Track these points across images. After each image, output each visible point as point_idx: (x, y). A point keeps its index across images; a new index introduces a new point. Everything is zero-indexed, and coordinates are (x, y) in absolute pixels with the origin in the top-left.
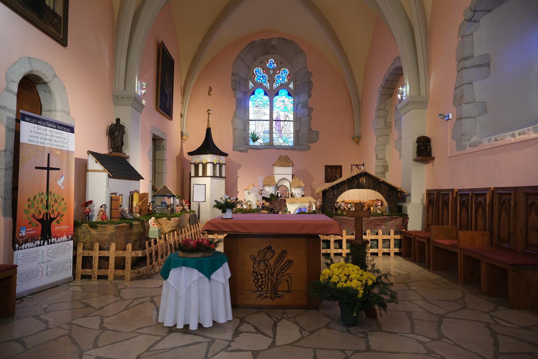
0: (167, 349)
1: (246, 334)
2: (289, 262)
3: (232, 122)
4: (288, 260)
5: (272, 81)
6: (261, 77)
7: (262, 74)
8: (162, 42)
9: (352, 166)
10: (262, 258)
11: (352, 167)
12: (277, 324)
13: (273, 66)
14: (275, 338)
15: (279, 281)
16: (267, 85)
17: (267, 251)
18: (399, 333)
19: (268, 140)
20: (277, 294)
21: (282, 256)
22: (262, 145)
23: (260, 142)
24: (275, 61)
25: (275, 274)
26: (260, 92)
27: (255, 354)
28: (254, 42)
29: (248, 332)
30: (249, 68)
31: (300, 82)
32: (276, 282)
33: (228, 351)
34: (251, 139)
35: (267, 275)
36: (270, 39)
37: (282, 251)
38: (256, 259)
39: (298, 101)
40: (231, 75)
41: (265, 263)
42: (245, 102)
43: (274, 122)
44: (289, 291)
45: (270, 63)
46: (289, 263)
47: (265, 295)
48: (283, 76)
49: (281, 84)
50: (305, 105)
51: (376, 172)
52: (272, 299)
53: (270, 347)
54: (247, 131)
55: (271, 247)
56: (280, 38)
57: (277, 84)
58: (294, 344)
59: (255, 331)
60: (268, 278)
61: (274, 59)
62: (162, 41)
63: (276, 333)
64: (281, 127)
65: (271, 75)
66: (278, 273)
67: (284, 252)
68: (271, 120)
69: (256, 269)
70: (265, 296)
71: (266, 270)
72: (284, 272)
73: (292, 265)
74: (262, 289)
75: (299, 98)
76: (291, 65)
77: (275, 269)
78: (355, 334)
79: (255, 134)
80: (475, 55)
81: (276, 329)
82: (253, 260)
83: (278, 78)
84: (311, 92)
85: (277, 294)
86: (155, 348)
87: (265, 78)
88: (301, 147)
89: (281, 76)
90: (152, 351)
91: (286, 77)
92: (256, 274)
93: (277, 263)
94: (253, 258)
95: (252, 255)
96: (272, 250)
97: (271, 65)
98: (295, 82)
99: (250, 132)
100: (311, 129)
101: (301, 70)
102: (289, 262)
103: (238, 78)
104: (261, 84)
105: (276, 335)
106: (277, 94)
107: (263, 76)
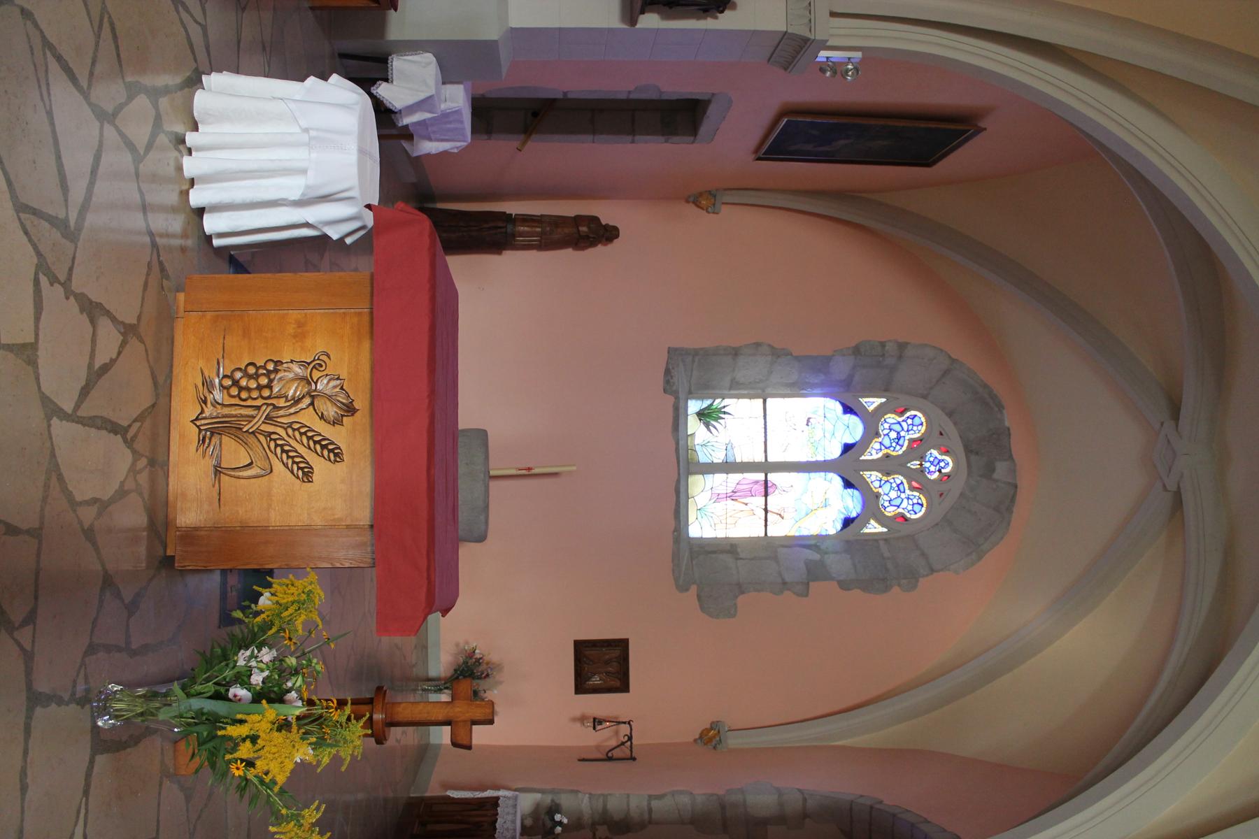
0: (50, 100)
1: (89, 336)
2: (306, 470)
3: (758, 345)
4: (311, 468)
5: (887, 465)
6: (898, 433)
7: (907, 437)
8: (980, 130)
9: (629, 723)
10: (318, 387)
11: (625, 723)
12: (119, 436)
13: (932, 468)
14: (73, 421)
15: (251, 439)
16: (873, 453)
17: (341, 403)
18: (87, 804)
19: (703, 459)
20: (212, 434)
21: (323, 447)
22: (689, 438)
24: (948, 476)
25: (270, 429)
26: (853, 429)
27: (27, 352)
28: (1001, 407)
29: (94, 341)
30: (925, 397)
31: (887, 554)
32: (247, 431)
33: (36, 274)
34: (707, 403)
35: (268, 405)
36: (1011, 458)
37: (339, 448)
38: (317, 369)
39: (827, 548)
40: (900, 340)
41: (303, 397)
42: (821, 385)
43: (761, 476)
44: (220, 472)
45: (940, 461)
46: (302, 469)
47: (210, 398)
49: (878, 496)
50: (816, 572)
51: (609, 797)
52: (197, 419)
53: (45, 400)
54: (732, 392)
55: (353, 415)
56: (1016, 487)
58: (53, 473)
59: (97, 366)
60: (258, 408)
61: (951, 471)
62: (985, 129)
63: (88, 426)
64: (745, 496)
65: (904, 465)
66: (274, 436)
67: (336, 455)
68: (767, 467)
69: (288, 370)
70: (205, 398)
71: (284, 399)
72: (276, 455)
73: (298, 478)
74: (227, 388)
75: (836, 553)
76: (937, 524)
77: (286, 426)
78: (84, 667)
79: (722, 416)
81: (103, 429)
82: (314, 360)
83: (898, 486)
84: (856, 590)
85: (212, 434)
86: (53, 65)
87: (894, 444)
88: (685, 562)
89: (903, 496)
90: (45, 54)
91: (900, 510)
92: (272, 369)
93: (305, 433)
94: (321, 360)
95: (328, 356)
96: (345, 418)
98: (886, 540)
99: (727, 401)
100: (743, 593)
101: (923, 554)
102: (306, 470)
104: (877, 435)
105: (84, 425)
106: (848, 484)
107: (902, 439)
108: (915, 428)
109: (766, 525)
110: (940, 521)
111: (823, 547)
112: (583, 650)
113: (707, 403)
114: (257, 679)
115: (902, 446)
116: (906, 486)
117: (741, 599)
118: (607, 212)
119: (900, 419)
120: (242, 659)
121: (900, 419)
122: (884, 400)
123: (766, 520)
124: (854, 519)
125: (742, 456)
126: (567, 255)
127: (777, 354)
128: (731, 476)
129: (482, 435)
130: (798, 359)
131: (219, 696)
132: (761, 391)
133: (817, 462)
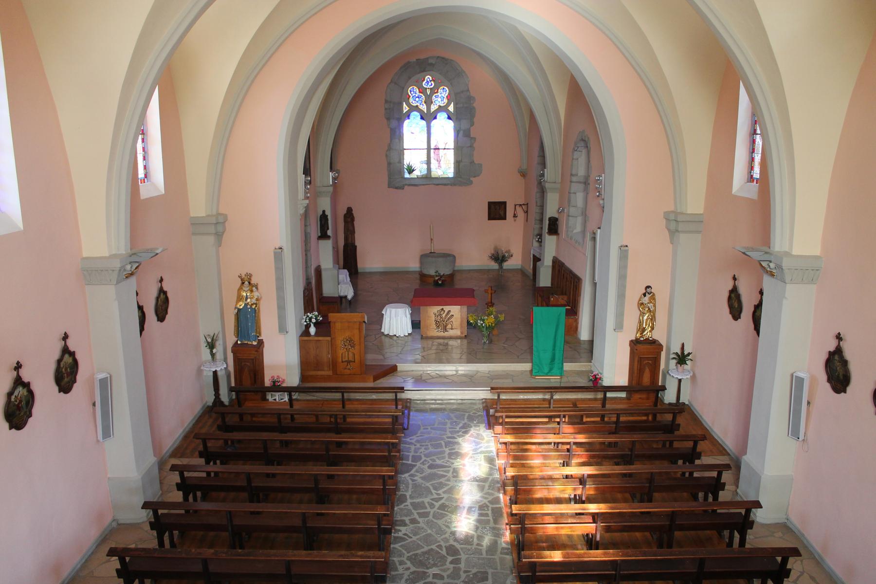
3: (387, 156)
5: (429, 102)
7: (418, 94)
13: (430, 84)
16: (424, 108)
24: (432, 78)
26: (415, 115)
28: (409, 62)
30: (403, 88)
31: (462, 105)
34: (406, 171)
40: (384, 101)
43: (432, 151)
45: (427, 81)
48: (441, 98)
56: (438, 57)
64: (439, 157)
68: (429, 149)
87: (421, 99)
89: (440, 96)
91: (445, 97)
97: (428, 82)
99: (405, 163)
100: (474, 161)
101: (462, 92)
103: (392, 105)
106: (435, 118)
108: (415, 91)
109: (450, 149)
110: (451, 84)
112: (491, 217)
114: (482, 323)
115: (421, 96)
116: (436, 94)
118: (342, 211)
119: (411, 96)
122: (404, 103)
123: (448, 149)
125: (425, 158)
126: (356, 223)
127: (390, 148)
128: (432, 162)
132: (401, 152)
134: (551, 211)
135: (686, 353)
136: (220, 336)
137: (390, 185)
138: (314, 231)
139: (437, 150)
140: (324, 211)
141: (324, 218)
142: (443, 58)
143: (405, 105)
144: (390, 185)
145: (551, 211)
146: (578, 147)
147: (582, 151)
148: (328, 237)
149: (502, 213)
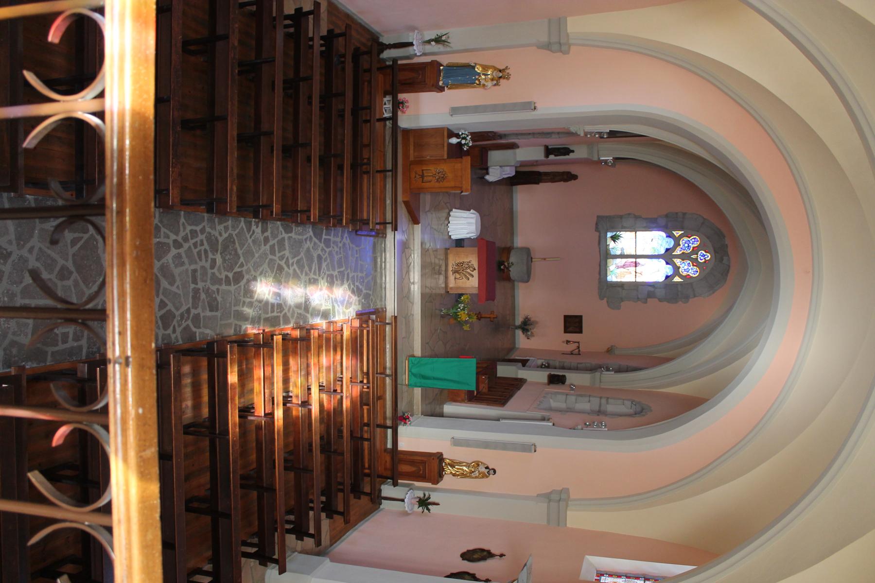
5: (684, 257)
7: (692, 246)
13: (702, 258)
16: (678, 252)
23: (612, 244)
24: (708, 260)
26: (671, 243)
28: (724, 237)
30: (698, 231)
31: (680, 289)
34: (614, 233)
36: (728, 256)
42: (655, 227)
43: (634, 260)
45: (705, 255)
48: (687, 269)
57: (679, 263)
68: (636, 257)
80: (608, 406)
89: (690, 268)
91: (688, 273)
97: (704, 256)
99: (622, 233)
100: (623, 301)
106: (667, 263)
108: (695, 243)
111: (656, 286)
113: (614, 233)
114: (461, 308)
116: (691, 264)
117: (622, 304)
119: (689, 239)
120: (459, 305)
121: (689, 239)
122: (683, 232)
124: (669, 276)
125: (626, 252)
127: (637, 217)
128: (623, 259)
129: (527, 251)
130: (646, 219)
131: (457, 310)
132: (634, 229)
133: (655, 255)
134: (572, 378)
135: (430, 507)
136: (448, 49)
137: (600, 219)
138: (554, 142)
139: (634, 264)
140: (573, 151)
141: (567, 151)
142: (728, 271)
143: (681, 232)
144: (600, 219)
145: (572, 378)
146: (635, 405)
147: (631, 409)
148: (547, 156)
149: (571, 329)
